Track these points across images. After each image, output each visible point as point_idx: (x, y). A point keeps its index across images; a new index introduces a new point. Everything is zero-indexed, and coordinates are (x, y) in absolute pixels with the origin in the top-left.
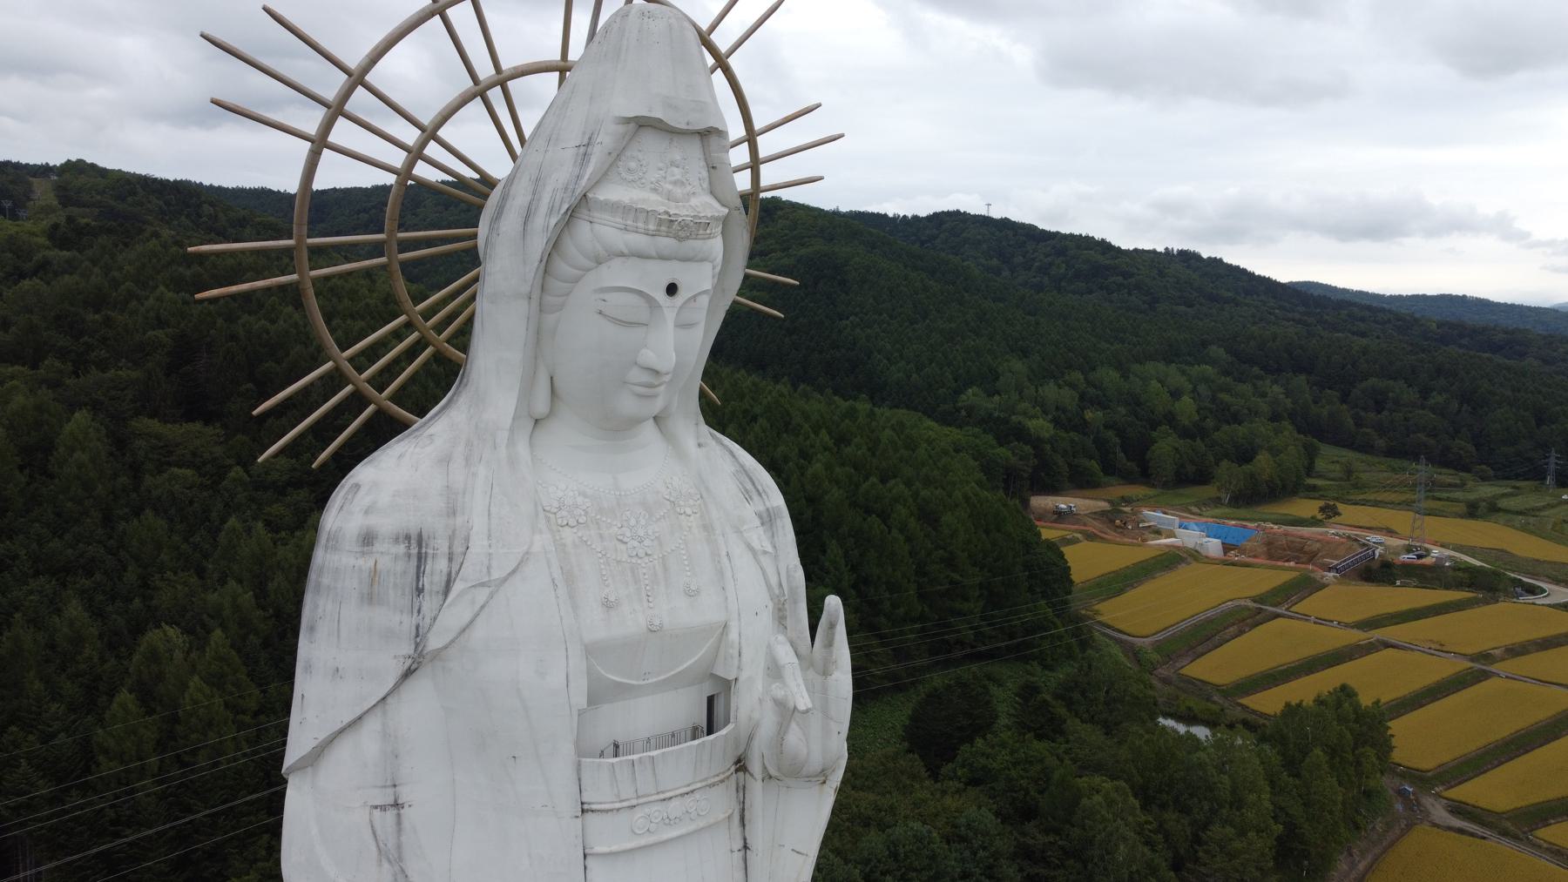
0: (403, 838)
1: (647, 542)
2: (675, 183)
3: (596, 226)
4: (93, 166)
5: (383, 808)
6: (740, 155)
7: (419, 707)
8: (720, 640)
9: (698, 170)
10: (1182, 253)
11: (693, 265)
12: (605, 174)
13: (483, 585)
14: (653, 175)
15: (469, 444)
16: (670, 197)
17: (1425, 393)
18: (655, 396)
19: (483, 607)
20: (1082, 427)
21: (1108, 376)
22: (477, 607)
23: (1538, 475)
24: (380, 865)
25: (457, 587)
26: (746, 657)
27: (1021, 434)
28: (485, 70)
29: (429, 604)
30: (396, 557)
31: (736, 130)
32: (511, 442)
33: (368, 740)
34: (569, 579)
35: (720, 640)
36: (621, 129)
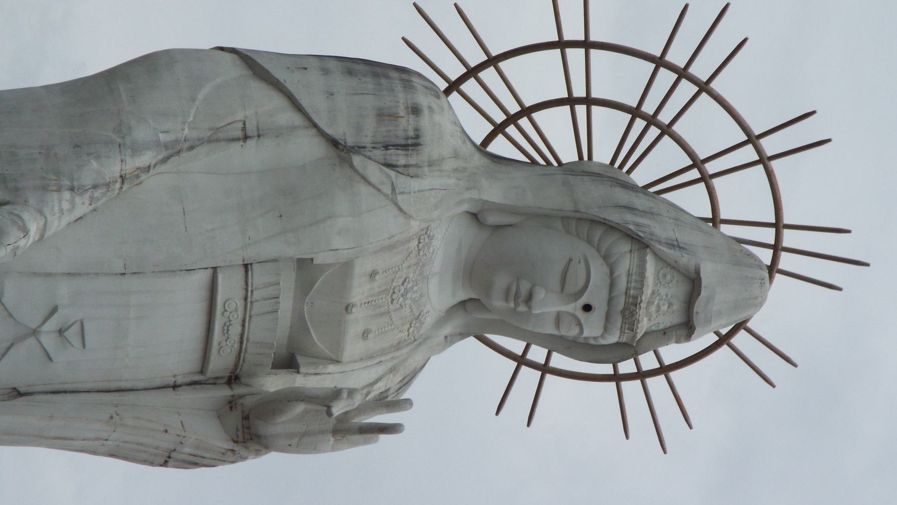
0: (223, 143)
1: (401, 299)
2: (658, 306)
3: (628, 255)
5: (244, 129)
6: (648, 361)
8: (326, 359)
11: (602, 324)
12: (665, 262)
13: (393, 189)
14: (663, 291)
15: (465, 169)
16: (649, 303)
18: (507, 299)
19: (379, 190)
22: (380, 187)
24: (210, 129)
25: (392, 174)
26: (400, 379)
28: (712, 168)
29: (378, 154)
30: (405, 130)
32: (471, 200)
34: (391, 247)
35: (326, 359)
36: (692, 269)
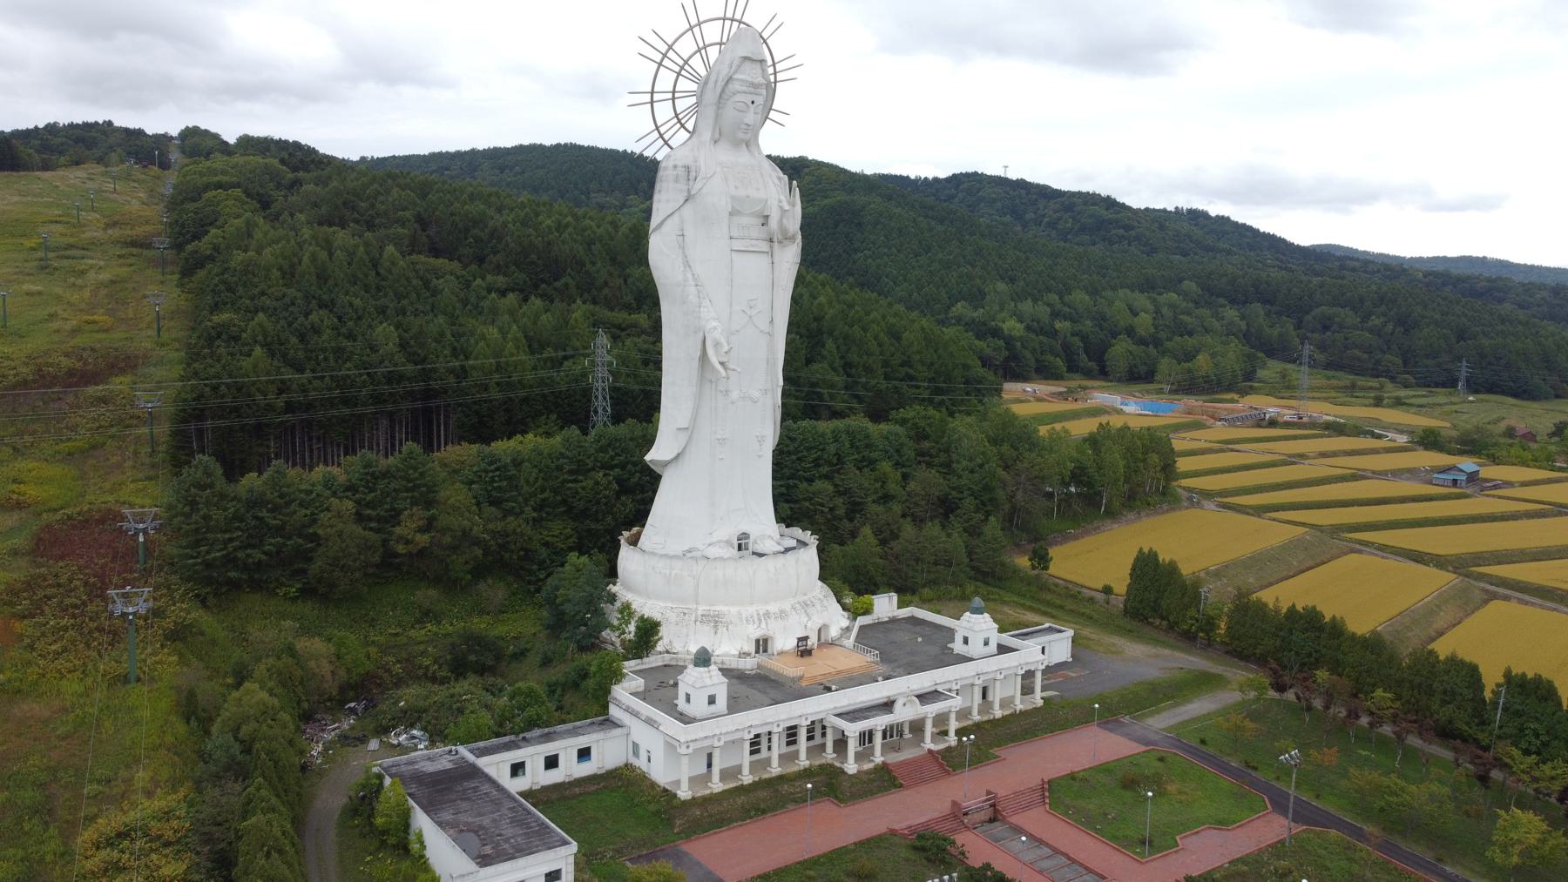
4: (206, 131)
6: (771, 70)
7: (688, 211)
9: (759, 71)
10: (1190, 211)
17: (1366, 317)
20: (1054, 333)
21: (1079, 297)
23: (1451, 383)
27: (996, 333)
31: (770, 62)
33: (676, 217)
